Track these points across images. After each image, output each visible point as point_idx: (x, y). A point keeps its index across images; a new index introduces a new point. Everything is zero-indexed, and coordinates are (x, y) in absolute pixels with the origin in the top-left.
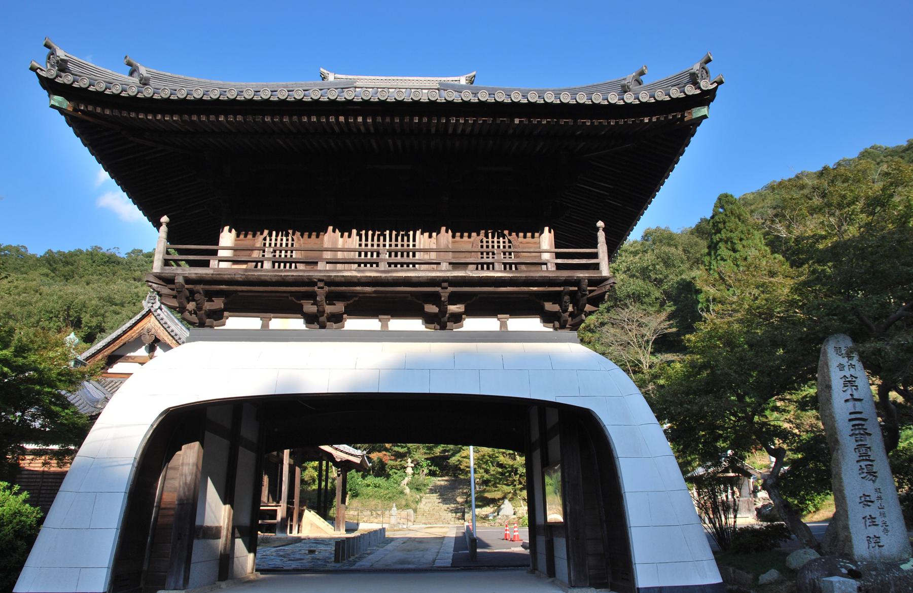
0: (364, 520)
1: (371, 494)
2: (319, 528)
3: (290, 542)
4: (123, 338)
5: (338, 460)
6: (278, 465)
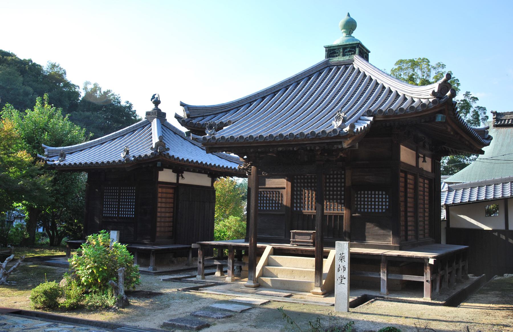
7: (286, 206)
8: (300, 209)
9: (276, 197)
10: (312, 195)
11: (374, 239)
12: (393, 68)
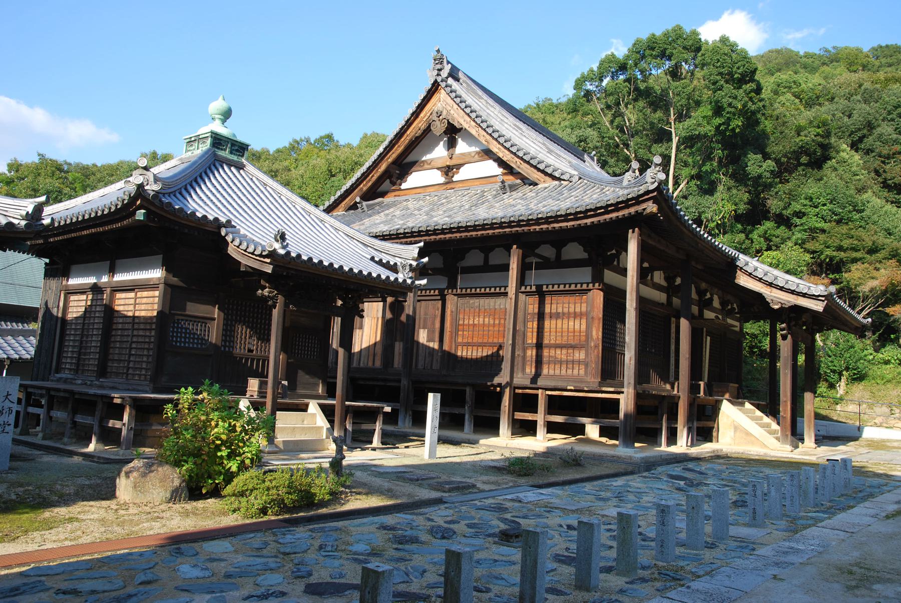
0: (876, 421)
1: (890, 376)
2: (751, 435)
3: (630, 469)
4: (408, 132)
5: (776, 307)
6: (670, 320)
7: (215, 345)
8: (229, 349)
9: (201, 330)
10: (246, 333)
11: (304, 388)
12: (155, 158)
